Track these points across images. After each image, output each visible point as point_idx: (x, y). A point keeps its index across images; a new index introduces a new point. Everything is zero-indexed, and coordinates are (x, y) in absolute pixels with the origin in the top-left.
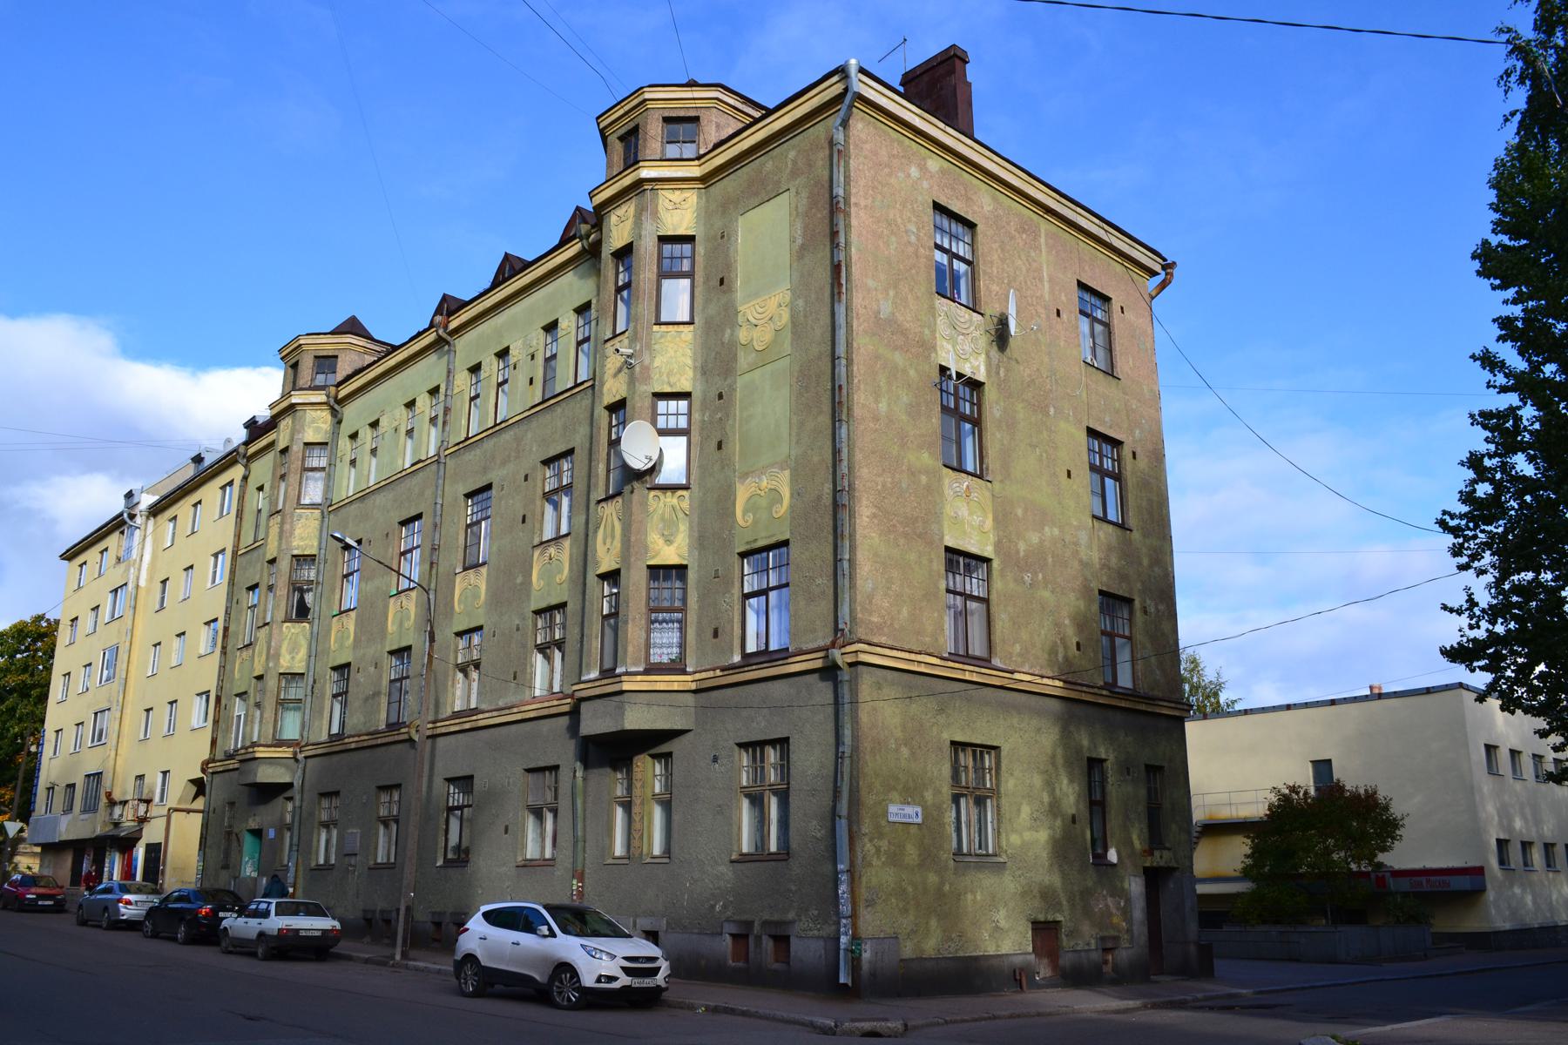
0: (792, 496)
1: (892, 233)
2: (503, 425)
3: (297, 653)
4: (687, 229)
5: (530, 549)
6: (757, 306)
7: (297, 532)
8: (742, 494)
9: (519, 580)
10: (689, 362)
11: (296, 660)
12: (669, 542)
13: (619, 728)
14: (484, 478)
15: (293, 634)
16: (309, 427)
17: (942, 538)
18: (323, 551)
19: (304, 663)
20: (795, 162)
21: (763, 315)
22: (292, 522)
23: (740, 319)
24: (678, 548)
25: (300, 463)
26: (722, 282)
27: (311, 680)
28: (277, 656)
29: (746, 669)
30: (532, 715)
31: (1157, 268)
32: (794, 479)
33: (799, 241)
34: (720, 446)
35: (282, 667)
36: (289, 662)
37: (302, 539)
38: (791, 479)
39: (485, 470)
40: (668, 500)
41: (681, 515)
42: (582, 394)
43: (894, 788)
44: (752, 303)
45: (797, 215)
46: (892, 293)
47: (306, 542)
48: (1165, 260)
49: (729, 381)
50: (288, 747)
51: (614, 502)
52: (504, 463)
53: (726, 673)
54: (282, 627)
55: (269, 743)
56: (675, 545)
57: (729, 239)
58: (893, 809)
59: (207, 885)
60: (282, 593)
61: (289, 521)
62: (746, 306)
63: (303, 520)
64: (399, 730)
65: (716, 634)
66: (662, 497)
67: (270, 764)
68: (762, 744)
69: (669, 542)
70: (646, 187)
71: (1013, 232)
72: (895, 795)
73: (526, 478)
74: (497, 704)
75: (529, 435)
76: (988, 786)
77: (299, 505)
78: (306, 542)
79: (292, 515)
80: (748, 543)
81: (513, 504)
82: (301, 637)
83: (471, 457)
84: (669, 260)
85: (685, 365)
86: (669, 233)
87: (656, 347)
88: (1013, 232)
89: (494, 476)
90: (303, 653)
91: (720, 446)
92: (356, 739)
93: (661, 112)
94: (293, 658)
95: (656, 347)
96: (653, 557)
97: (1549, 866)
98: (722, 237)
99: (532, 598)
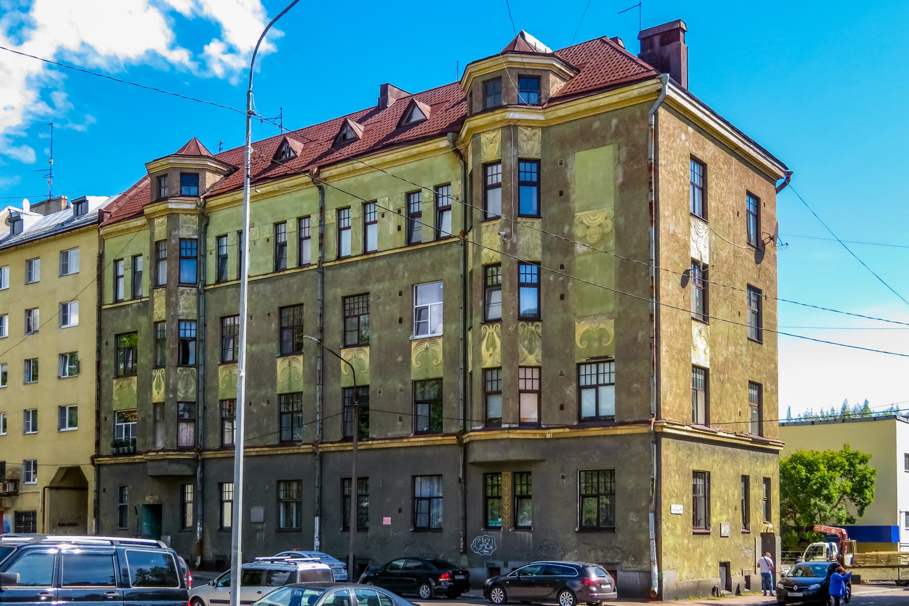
0: (616, 334)
1: (674, 180)
2: (372, 256)
3: (189, 388)
4: (536, 154)
8: (581, 328)
9: (400, 359)
10: (539, 242)
12: (531, 352)
14: (361, 288)
15: (185, 375)
16: (183, 227)
17: (691, 360)
18: (202, 318)
19: (195, 395)
20: (617, 127)
21: (594, 222)
22: (177, 297)
23: (576, 221)
24: (536, 356)
25: (178, 253)
26: (561, 193)
27: (201, 407)
30: (419, 444)
31: (782, 174)
32: (616, 326)
33: (620, 180)
34: (562, 297)
35: (180, 397)
36: (184, 394)
37: (185, 308)
39: (362, 283)
40: (530, 327)
41: (537, 337)
43: (673, 497)
45: (619, 162)
46: (674, 217)
47: (189, 310)
48: (786, 168)
49: (568, 258)
51: (495, 326)
52: (379, 280)
54: (176, 371)
55: (175, 449)
56: (535, 354)
58: (673, 507)
60: (174, 346)
61: (175, 295)
62: (581, 214)
63: (185, 295)
66: (526, 326)
69: (531, 352)
72: (673, 500)
73: (400, 294)
74: (387, 435)
75: (401, 266)
76: (352, 448)
77: (180, 284)
79: (176, 291)
81: (390, 310)
82: (191, 378)
83: (347, 272)
84: (524, 173)
85: (537, 244)
86: (525, 157)
87: (520, 232)
89: (373, 288)
90: (193, 389)
91: (562, 297)
93: (517, 71)
94: (187, 392)
95: (520, 232)
96: (522, 362)
97: (696, 522)
98: (561, 164)
99: (412, 372)
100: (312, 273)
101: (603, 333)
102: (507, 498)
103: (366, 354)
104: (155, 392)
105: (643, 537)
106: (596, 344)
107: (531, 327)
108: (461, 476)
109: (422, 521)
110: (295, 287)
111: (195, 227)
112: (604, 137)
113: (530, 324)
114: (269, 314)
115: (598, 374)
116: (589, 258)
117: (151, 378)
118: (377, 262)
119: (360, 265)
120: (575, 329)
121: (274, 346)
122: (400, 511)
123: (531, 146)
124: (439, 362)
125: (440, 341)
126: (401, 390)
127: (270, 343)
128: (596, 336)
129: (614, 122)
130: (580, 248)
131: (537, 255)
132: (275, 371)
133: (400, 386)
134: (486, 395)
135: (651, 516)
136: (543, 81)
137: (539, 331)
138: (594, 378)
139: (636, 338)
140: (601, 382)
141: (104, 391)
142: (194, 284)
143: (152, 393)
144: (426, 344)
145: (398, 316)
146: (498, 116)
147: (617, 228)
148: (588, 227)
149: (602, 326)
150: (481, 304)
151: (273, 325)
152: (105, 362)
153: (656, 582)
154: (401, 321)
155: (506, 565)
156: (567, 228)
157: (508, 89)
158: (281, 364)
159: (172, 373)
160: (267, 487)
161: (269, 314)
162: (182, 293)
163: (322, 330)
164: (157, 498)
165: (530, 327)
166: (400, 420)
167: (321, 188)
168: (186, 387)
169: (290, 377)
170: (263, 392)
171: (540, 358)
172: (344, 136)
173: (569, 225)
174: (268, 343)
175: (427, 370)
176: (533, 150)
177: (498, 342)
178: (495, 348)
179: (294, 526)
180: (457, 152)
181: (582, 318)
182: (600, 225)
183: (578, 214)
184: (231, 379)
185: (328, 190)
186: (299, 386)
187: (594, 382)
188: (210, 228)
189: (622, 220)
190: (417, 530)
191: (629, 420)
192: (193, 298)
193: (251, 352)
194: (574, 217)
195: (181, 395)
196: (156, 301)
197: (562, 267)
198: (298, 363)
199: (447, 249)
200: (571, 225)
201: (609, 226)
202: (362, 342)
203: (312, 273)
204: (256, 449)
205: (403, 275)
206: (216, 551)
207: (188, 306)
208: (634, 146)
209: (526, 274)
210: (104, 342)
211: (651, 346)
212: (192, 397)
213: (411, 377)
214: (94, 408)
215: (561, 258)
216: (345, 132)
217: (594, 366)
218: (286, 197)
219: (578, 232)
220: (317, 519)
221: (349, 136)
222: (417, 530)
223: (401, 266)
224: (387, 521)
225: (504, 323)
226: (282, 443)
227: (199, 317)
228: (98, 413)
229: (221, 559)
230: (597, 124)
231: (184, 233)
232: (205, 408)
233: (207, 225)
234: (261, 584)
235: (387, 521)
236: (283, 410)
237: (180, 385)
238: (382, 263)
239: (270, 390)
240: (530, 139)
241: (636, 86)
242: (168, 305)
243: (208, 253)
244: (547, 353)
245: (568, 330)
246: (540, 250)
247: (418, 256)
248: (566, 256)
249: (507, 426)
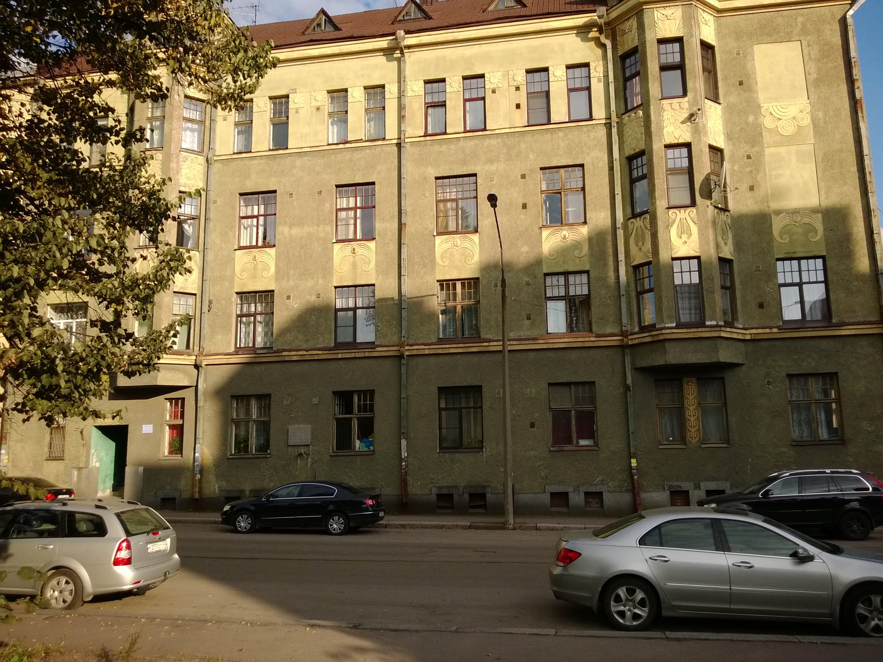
0: (825, 230)
5: (538, 231)
6: (779, 107)
7: (184, 171)
11: (188, 282)
13: (714, 360)
14: (465, 168)
22: (178, 162)
26: (741, 83)
29: (802, 330)
30: (561, 346)
34: (752, 188)
38: (823, 220)
42: (590, 128)
44: (772, 104)
47: (193, 182)
50: (189, 356)
52: (490, 161)
53: (781, 331)
57: (745, 57)
59: (712, 541)
63: (188, 163)
64: (375, 348)
65: (761, 306)
66: (678, 212)
67: (170, 369)
68: (248, 397)
70: (693, 3)
71: (85, 298)
73: (523, 176)
75: (523, 146)
78: (193, 182)
79: (178, 156)
80: (786, 253)
88: (85, 298)
91: (752, 188)
92: (301, 353)
101: (812, 229)
102: (692, 408)
103: (474, 242)
112: (790, 33)
113: (722, 213)
114: (320, 192)
115: (800, 271)
119: (462, 143)
120: (771, 222)
124: (584, 253)
126: (528, 284)
127: (322, 226)
132: (331, 259)
133: (526, 279)
138: (796, 275)
142: (429, 107)
145: (521, 202)
147: (814, 121)
154: (524, 206)
155: (697, 487)
156: (751, 119)
160: (315, 400)
161: (320, 192)
165: (723, 216)
166: (529, 318)
170: (310, 283)
173: (755, 115)
174: (318, 226)
177: (694, 229)
179: (254, 452)
182: (794, 118)
184: (255, 268)
187: (797, 280)
191: (852, 321)
193: (291, 236)
197: (749, 157)
199: (588, 131)
201: (806, 121)
204: (301, 353)
206: (224, 484)
207: (192, 176)
213: (542, 269)
215: (747, 148)
219: (768, 122)
225: (700, 208)
226: (339, 346)
229: (480, 491)
234: (100, 521)
238: (493, 142)
239: (321, 281)
247: (548, 136)
248: (753, 147)
249: (714, 323)
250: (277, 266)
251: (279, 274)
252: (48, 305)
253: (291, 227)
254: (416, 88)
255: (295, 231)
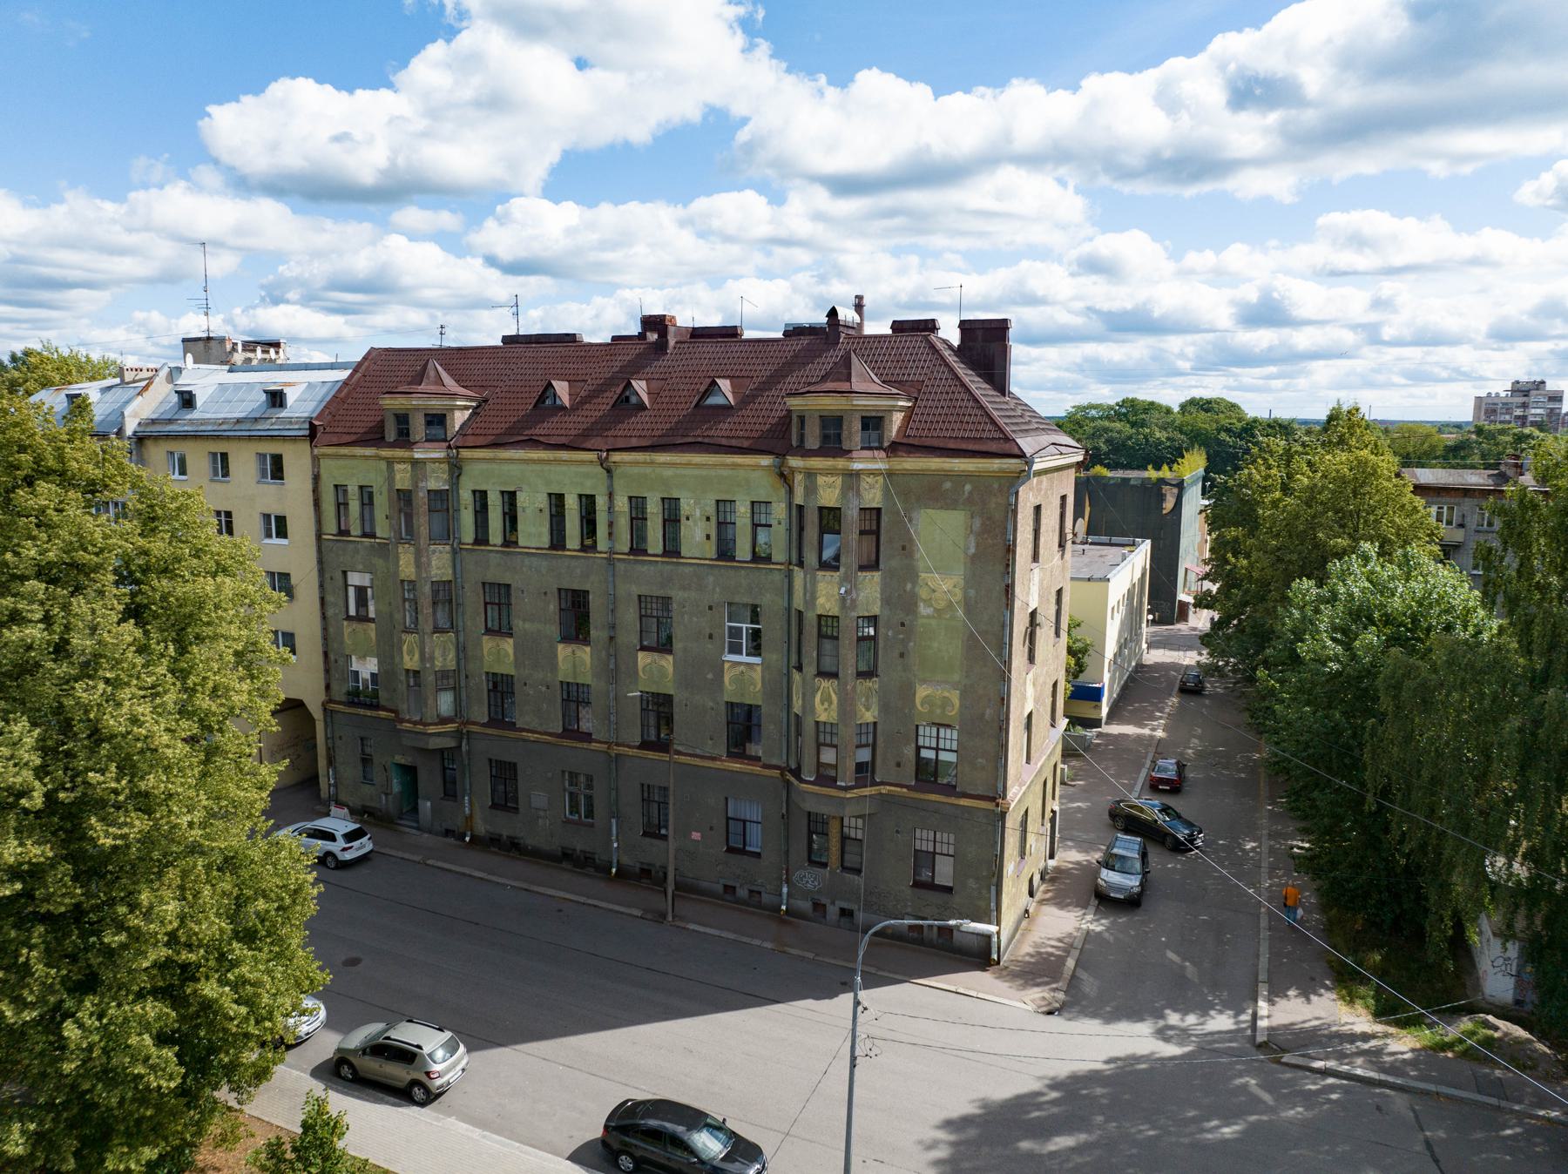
0: (961, 706)
8: (922, 692)
9: (710, 676)
12: (868, 710)
23: (920, 582)
26: (904, 548)
28: (432, 659)
32: (963, 697)
33: (972, 550)
34: (902, 655)
52: (684, 588)
73: (710, 608)
75: (711, 579)
79: (427, 551)
90: (452, 655)
91: (902, 655)
100: (599, 561)
101: (946, 702)
104: (406, 658)
105: (982, 904)
106: (938, 711)
107: (869, 684)
108: (784, 811)
109: (736, 843)
110: (578, 571)
111: (445, 476)
116: (933, 622)
117: (401, 642)
118: (681, 568)
119: (660, 566)
121: (553, 630)
122: (711, 828)
123: (873, 495)
125: (759, 669)
128: (939, 703)
129: (968, 487)
130: (924, 610)
131: (876, 610)
132: (556, 656)
133: (711, 704)
134: (819, 745)
135: (993, 889)
136: (887, 422)
137: (876, 686)
139: (983, 714)
140: (941, 746)
141: (331, 630)
143: (402, 658)
144: (742, 668)
145: (708, 631)
146: (840, 463)
148: (934, 591)
149: (946, 694)
150: (815, 654)
151: (552, 607)
152: (330, 598)
153: (994, 949)
154: (711, 637)
155: (833, 903)
156: (909, 586)
157: (850, 433)
158: (563, 651)
159: (427, 639)
162: (434, 552)
163: (613, 627)
164: (410, 759)
167: (609, 471)
168: (444, 655)
169: (574, 666)
171: (876, 713)
172: (627, 399)
175: (742, 695)
176: (874, 499)
178: (831, 703)
180: (782, 475)
181: (924, 681)
183: (923, 575)
185: (617, 472)
186: (586, 678)
187: (934, 745)
188: (463, 479)
189: (972, 593)
190: (730, 850)
192: (447, 557)
194: (918, 576)
195: (438, 664)
196: (402, 556)
197: (903, 625)
198: (585, 653)
200: (914, 583)
202: (665, 646)
203: (599, 561)
205: (714, 589)
208: (989, 518)
209: (937, 749)
210: (327, 576)
211: (1000, 728)
212: (451, 665)
214: (320, 650)
216: (627, 393)
217: (934, 730)
218: (564, 468)
219: (923, 593)
220: (614, 821)
221: (633, 400)
222: (730, 850)
223: (711, 579)
224: (696, 836)
227: (456, 578)
228: (326, 654)
230: (948, 485)
231: (433, 484)
232: (467, 677)
233: (460, 475)
235: (696, 836)
236: (488, 600)
237: (437, 653)
238: (687, 570)
240: (872, 487)
241: (997, 461)
242: (418, 564)
243: (462, 508)
244: (885, 708)
245: (908, 692)
246: (879, 603)
250: (515, 653)
251: (518, 663)
252: (372, 620)
253: (524, 620)
254: (622, 504)
255: (527, 626)
